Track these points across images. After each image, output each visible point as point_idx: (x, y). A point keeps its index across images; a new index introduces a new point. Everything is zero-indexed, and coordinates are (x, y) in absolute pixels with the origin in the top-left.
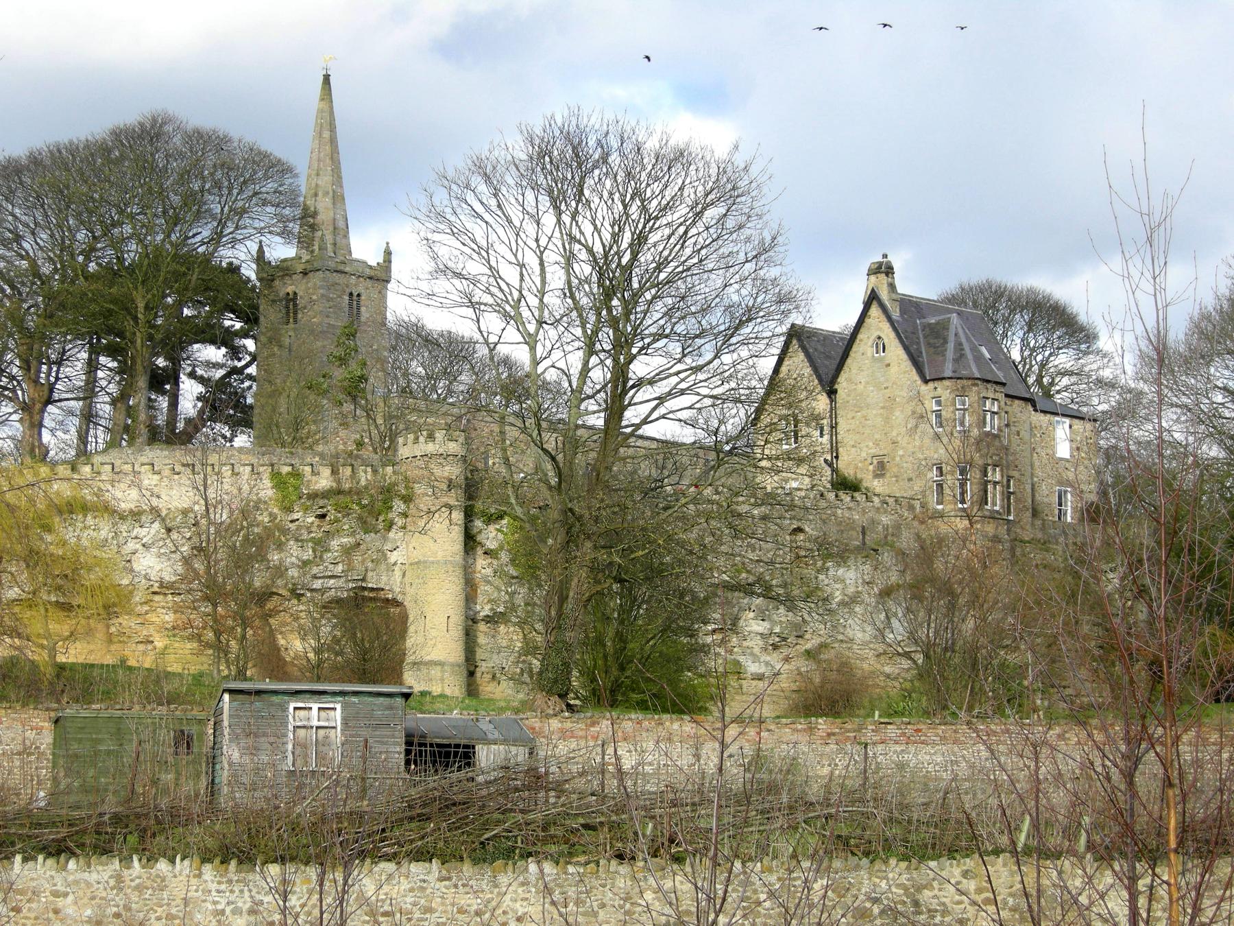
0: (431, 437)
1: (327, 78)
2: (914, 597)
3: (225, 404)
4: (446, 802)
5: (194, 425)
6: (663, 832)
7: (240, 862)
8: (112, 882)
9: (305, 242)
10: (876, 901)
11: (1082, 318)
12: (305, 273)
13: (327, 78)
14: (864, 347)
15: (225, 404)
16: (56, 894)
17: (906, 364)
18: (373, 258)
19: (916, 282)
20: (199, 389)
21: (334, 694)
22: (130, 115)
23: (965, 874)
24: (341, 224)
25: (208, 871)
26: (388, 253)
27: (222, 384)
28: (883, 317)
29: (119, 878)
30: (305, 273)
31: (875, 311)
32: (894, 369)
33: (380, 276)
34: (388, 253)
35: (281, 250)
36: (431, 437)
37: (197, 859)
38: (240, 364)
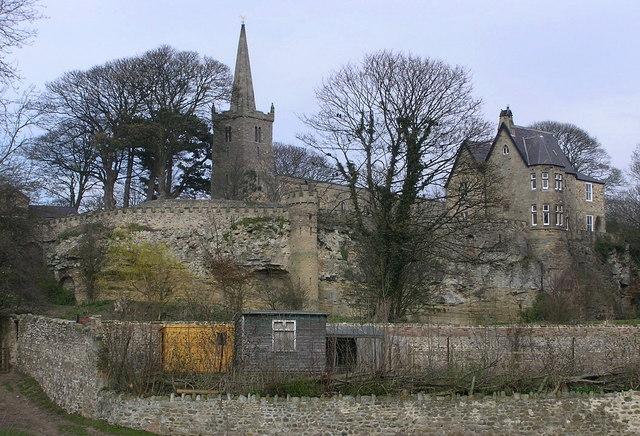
0: (301, 195)
1: (243, 26)
2: (524, 266)
3: (193, 180)
4: (341, 369)
5: (180, 189)
6: (445, 384)
7: (279, 396)
8: (218, 406)
9: (234, 101)
10: (583, 412)
11: (591, 135)
12: (234, 118)
13: (243, 26)
14: (499, 147)
15: (193, 180)
16: (190, 412)
17: (519, 159)
18: (266, 111)
19: (521, 120)
20: (182, 172)
21: (293, 315)
22: (153, 46)
23: (627, 399)
24: (251, 94)
25: (264, 401)
26: (273, 108)
27: (191, 170)
28: (507, 136)
29: (221, 404)
30: (234, 118)
31: (503, 134)
32: (512, 160)
33: (269, 119)
34: (273, 108)
35: (224, 106)
36: (301, 195)
37: (258, 396)
38: (201, 160)
